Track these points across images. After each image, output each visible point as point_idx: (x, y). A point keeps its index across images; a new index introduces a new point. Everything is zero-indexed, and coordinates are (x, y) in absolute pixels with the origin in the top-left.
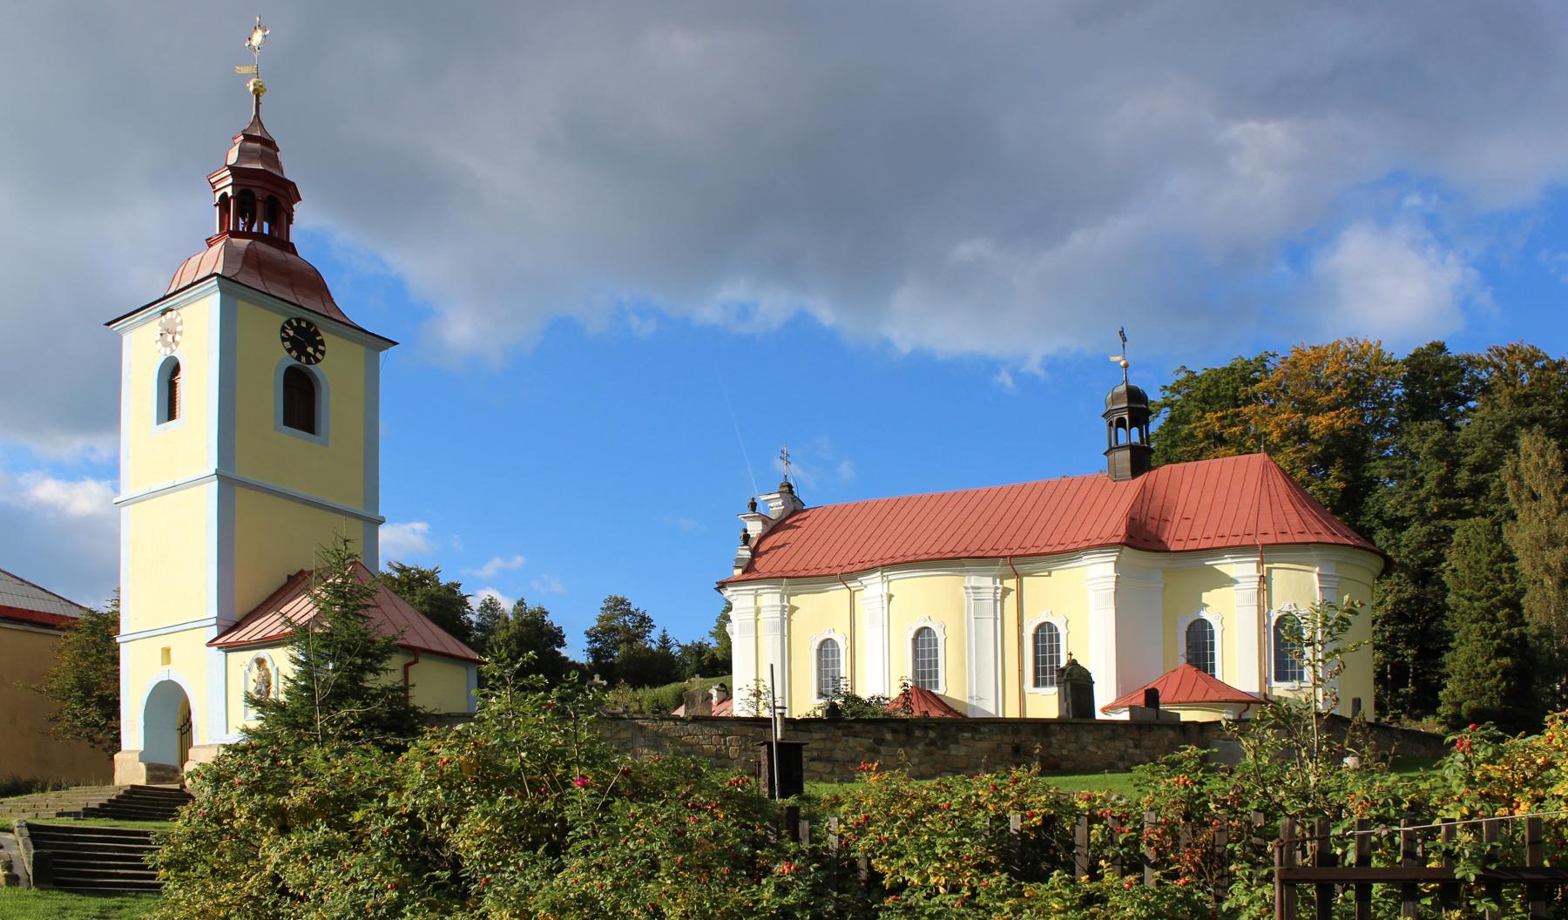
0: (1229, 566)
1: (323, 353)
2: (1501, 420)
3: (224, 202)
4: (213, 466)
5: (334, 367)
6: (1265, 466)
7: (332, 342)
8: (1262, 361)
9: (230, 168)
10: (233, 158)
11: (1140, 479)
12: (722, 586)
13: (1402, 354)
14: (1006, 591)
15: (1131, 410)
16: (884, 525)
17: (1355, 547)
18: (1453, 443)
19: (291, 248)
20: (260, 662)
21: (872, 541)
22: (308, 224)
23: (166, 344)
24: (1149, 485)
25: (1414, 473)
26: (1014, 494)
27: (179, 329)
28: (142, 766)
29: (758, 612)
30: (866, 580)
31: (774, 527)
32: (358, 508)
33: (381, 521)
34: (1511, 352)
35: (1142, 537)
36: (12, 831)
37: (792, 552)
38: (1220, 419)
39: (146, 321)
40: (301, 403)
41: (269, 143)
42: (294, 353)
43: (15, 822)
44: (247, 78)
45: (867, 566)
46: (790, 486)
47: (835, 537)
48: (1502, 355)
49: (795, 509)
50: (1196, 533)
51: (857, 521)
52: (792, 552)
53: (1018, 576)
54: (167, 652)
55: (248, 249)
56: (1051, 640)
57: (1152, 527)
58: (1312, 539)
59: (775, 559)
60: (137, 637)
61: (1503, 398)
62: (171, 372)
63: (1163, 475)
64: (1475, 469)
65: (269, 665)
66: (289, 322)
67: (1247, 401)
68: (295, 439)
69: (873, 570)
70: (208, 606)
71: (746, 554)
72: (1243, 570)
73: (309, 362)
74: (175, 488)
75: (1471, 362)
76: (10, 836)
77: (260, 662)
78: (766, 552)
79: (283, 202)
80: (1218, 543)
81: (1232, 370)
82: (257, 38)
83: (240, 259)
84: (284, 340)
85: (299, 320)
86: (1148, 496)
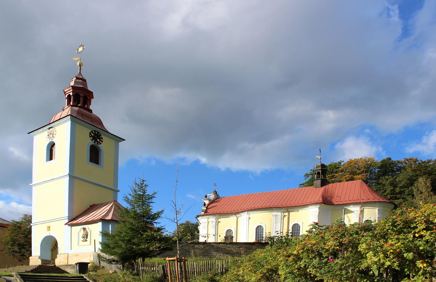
0: (351, 208)
1: (102, 141)
2: (409, 175)
3: (69, 97)
4: (67, 172)
5: (105, 146)
6: (361, 183)
7: (105, 138)
8: (340, 163)
10: (72, 84)
11: (323, 187)
12: (198, 216)
14: (285, 216)
15: (322, 170)
17: (389, 202)
18: (395, 181)
19: (91, 111)
20: (84, 229)
22: (96, 107)
23: (50, 138)
25: (383, 189)
26: (285, 192)
28: (40, 260)
30: (242, 214)
31: (212, 202)
32: (112, 187)
33: (119, 191)
34: (410, 159)
35: (326, 201)
36: (13, 276)
39: (42, 132)
40: (95, 156)
41: (84, 80)
42: (93, 141)
43: (13, 273)
44: (77, 61)
45: (243, 210)
46: (216, 192)
47: (231, 204)
49: (217, 198)
50: (342, 200)
51: (237, 200)
53: (289, 212)
57: (329, 199)
59: (213, 210)
60: (37, 224)
61: (409, 170)
62: (51, 147)
64: (401, 187)
65: (87, 229)
66: (92, 132)
67: (336, 172)
68: (93, 166)
69: (245, 211)
70: (66, 214)
72: (356, 209)
73: (98, 144)
75: (399, 162)
76: (12, 278)
77: (84, 229)
79: (89, 98)
82: (81, 49)
84: (90, 137)
85: (95, 131)
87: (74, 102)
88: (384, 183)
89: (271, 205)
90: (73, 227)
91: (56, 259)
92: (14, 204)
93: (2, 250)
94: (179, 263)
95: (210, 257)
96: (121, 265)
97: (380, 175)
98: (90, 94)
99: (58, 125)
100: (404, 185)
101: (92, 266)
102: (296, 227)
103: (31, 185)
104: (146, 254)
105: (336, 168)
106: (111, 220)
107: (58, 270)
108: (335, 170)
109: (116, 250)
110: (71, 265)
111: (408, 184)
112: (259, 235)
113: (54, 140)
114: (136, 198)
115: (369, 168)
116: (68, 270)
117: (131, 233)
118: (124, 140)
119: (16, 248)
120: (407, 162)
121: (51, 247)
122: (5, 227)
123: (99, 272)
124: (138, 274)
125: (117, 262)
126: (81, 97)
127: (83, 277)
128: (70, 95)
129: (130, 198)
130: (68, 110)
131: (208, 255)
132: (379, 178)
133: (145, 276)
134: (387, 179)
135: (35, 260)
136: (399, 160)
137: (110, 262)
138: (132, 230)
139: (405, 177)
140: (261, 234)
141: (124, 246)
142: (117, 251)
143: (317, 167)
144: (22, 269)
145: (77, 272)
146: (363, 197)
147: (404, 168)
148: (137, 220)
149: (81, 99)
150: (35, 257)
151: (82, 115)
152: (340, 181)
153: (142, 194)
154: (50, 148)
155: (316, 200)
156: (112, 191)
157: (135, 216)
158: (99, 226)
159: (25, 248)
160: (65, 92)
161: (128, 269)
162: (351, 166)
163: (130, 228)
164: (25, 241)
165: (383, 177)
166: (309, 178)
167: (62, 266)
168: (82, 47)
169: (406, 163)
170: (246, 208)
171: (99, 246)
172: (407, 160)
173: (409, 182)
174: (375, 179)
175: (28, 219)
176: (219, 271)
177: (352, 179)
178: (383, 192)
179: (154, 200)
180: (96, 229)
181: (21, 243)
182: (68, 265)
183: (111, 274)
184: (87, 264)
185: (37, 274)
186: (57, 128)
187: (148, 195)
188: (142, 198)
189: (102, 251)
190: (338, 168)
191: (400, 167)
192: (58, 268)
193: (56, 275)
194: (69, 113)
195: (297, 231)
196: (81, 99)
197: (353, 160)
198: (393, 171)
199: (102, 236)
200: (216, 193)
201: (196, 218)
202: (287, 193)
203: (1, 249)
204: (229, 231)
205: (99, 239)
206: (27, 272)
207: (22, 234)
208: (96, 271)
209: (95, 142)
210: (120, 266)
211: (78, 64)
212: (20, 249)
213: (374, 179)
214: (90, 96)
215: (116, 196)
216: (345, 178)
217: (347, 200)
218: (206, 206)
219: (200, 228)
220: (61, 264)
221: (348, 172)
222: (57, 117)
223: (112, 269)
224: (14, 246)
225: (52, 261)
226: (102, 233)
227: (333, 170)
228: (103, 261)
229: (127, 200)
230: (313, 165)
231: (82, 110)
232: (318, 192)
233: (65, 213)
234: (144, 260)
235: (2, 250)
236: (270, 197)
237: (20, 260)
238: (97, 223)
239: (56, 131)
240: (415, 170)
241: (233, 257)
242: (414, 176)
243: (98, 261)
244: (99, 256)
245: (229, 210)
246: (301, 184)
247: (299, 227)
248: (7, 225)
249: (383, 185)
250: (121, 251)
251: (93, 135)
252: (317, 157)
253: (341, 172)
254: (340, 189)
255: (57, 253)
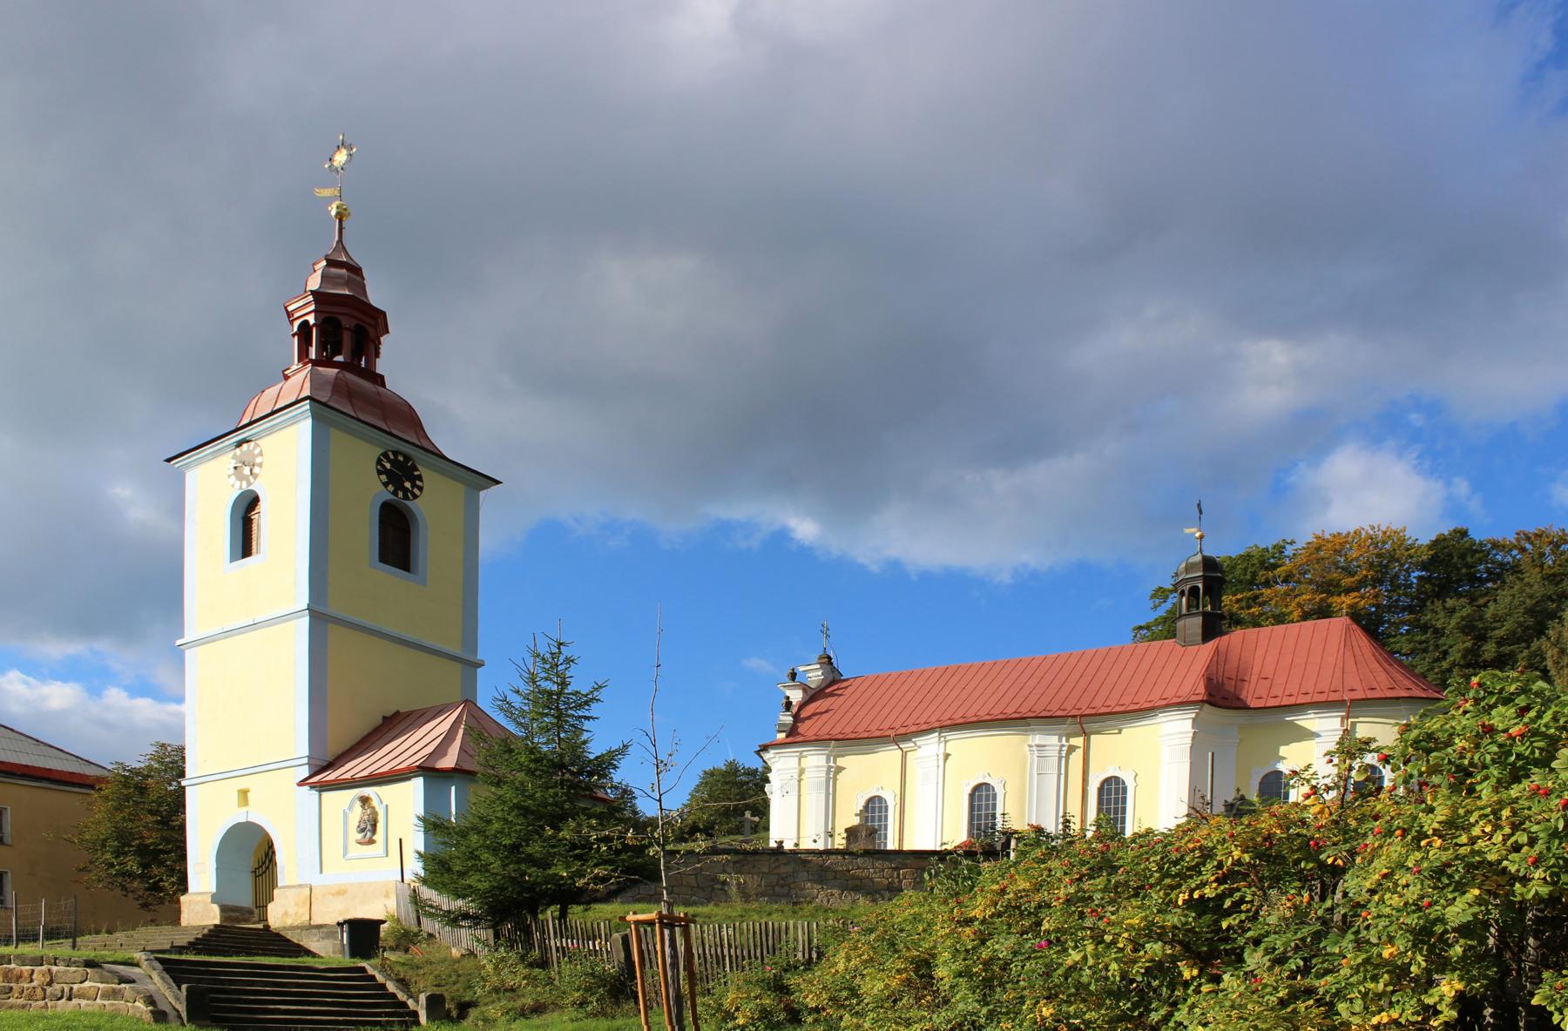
0: (1310, 721)
1: (421, 489)
2: (1531, 597)
3: (304, 332)
4: (303, 601)
5: (432, 504)
6: (1348, 629)
8: (1280, 549)
9: (313, 292)
10: (314, 283)
11: (1212, 644)
12: (765, 748)
13: (1425, 538)
14: (1072, 749)
15: (1205, 578)
16: (934, 691)
18: (1481, 618)
19: (379, 380)
20: (365, 800)
21: (923, 706)
22: (399, 364)
23: (241, 477)
24: (1222, 649)
25: (1437, 646)
26: (1073, 661)
27: (258, 460)
28: (216, 909)
29: (802, 772)
30: (920, 741)
31: (813, 696)
32: (456, 650)
33: (481, 665)
34: (1538, 536)
35: (1221, 696)
36: (137, 965)
37: (837, 717)
38: (1238, 601)
39: (215, 455)
40: (397, 540)
41: (356, 270)
42: (391, 488)
43: (138, 956)
44: (330, 200)
45: (925, 727)
48: (1528, 539)
49: (834, 681)
50: (1277, 691)
52: (837, 717)
53: (1086, 734)
54: (244, 795)
55: (337, 378)
56: (1117, 793)
57: (1230, 686)
58: (1404, 694)
59: (819, 724)
60: (203, 780)
61: (1532, 576)
62: (247, 507)
63: (1236, 638)
64: (1501, 642)
65: (375, 803)
66: (385, 455)
67: (1267, 584)
68: (390, 576)
69: (930, 731)
70: (299, 745)
71: (788, 719)
72: (1327, 726)
74: (254, 626)
75: (1495, 545)
76: (136, 970)
77: (365, 800)
78: (809, 718)
79: (371, 331)
80: (1301, 699)
81: (1249, 556)
82: (341, 158)
83: (329, 388)
84: (380, 473)
85: (396, 453)
86: (1222, 658)
87: (321, 347)
88: (1439, 625)
89: (1024, 710)
90: (325, 795)
91: (270, 906)
92: (115, 696)
93: (84, 869)
94: (666, 932)
95: (795, 904)
96: (491, 932)
97: (1425, 593)
98: (376, 319)
99: (270, 431)
100: (1514, 633)
101: (392, 932)
102: (1113, 793)
103: (179, 642)
104: (567, 896)
105: (1267, 569)
106: (454, 770)
107: (278, 943)
108: (1262, 575)
109: (472, 880)
110: (321, 926)
111: (1527, 628)
112: (979, 817)
113: (257, 487)
114: (535, 702)
115: (1386, 566)
116: (313, 944)
117: (519, 823)
118: (498, 482)
119: (133, 865)
120: (1528, 546)
121: (252, 863)
122: (92, 787)
123: (418, 952)
124: (544, 964)
125: (475, 920)
126: (345, 330)
127: (363, 970)
128: (306, 322)
129: (517, 701)
130: (300, 380)
131: (788, 895)
132: (1423, 605)
133: (567, 969)
134: (1452, 611)
135: (201, 902)
136: (1498, 536)
137: (453, 919)
138: (525, 811)
139: (1516, 602)
140: (987, 816)
141: (496, 866)
142: (475, 884)
143: (1189, 568)
144: (162, 937)
145: (343, 952)
146: (1353, 680)
147: (1516, 569)
148: (541, 777)
149: (347, 339)
150: (199, 898)
151: (350, 394)
152: (1280, 619)
153: (555, 688)
154: (241, 513)
155: (1185, 693)
156: (458, 666)
157: (532, 765)
158: (415, 788)
159: (161, 863)
160: (289, 314)
161: (511, 945)
162: (1318, 561)
163: (517, 806)
164: (164, 839)
165: (1438, 604)
166: (1168, 605)
167: (293, 928)
168: (344, 152)
169: (1523, 550)
170: (933, 719)
171: (415, 867)
172: (1528, 539)
173: (1530, 621)
174: (1410, 609)
175: (172, 763)
176: (800, 955)
177: (1324, 612)
178: (1437, 660)
179: (595, 709)
180: (404, 804)
181: (147, 846)
182: (310, 928)
183: (458, 961)
184: (376, 924)
185: (214, 959)
186: (265, 443)
187: (577, 693)
188: (558, 705)
189: (424, 881)
190: (1275, 567)
191: (1502, 565)
192: (278, 935)
193: (273, 961)
194: (306, 392)
195: (1116, 802)
196: (347, 339)
197: (1327, 536)
198: (1473, 579)
199: (426, 832)
200: (827, 661)
201: (758, 753)
202: (1082, 665)
203: (82, 865)
204: (874, 807)
205: (416, 841)
206: (180, 950)
207: (151, 812)
208: (407, 951)
209: (395, 493)
210: (486, 934)
211: (333, 213)
212: (145, 866)
213: (1404, 609)
214: (375, 327)
215: (470, 684)
216: (1299, 605)
217: (1295, 692)
218: (794, 710)
219: (774, 790)
220: (289, 922)
221: (1311, 582)
222: (265, 404)
223: (458, 943)
224: (125, 854)
225: (256, 911)
226: (424, 820)
227: (1254, 574)
228: (431, 915)
229: (506, 707)
230: (1171, 558)
231: (350, 377)
232: (1191, 661)
233: (296, 742)
234: (563, 914)
235: (84, 869)
236: (1023, 680)
237: (145, 906)
238: (409, 779)
239: (261, 454)
240: (1554, 575)
241: (874, 901)
242: (1550, 598)
243: (413, 916)
244: (415, 898)
245: (873, 727)
246: (1141, 628)
247: (1125, 790)
248: (100, 780)
249: (1436, 631)
250: (486, 885)
251: (388, 466)
252: (1187, 531)
253: (1285, 581)
254: (1270, 652)
255: (272, 884)
